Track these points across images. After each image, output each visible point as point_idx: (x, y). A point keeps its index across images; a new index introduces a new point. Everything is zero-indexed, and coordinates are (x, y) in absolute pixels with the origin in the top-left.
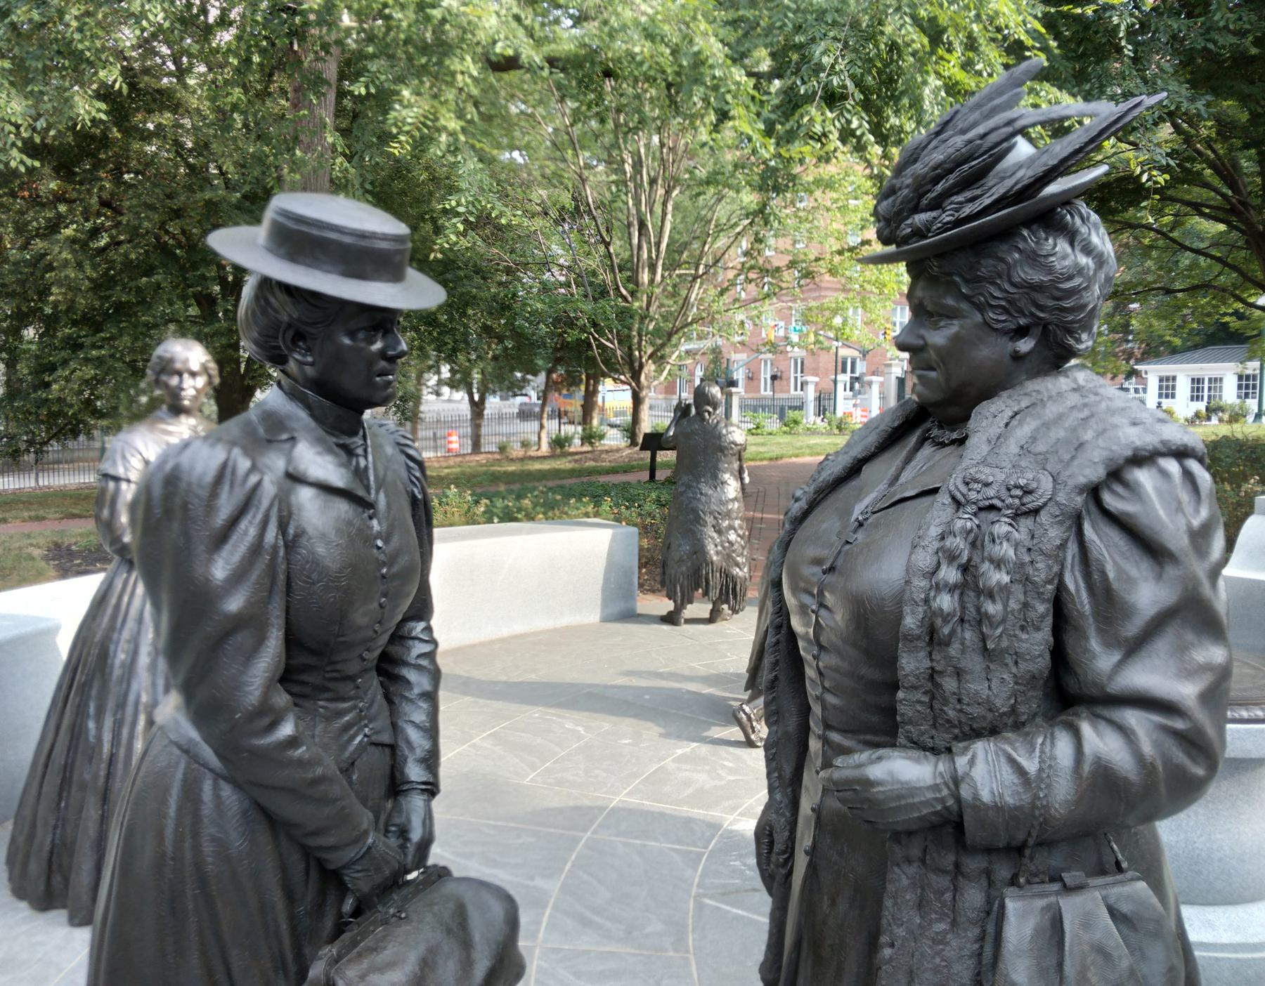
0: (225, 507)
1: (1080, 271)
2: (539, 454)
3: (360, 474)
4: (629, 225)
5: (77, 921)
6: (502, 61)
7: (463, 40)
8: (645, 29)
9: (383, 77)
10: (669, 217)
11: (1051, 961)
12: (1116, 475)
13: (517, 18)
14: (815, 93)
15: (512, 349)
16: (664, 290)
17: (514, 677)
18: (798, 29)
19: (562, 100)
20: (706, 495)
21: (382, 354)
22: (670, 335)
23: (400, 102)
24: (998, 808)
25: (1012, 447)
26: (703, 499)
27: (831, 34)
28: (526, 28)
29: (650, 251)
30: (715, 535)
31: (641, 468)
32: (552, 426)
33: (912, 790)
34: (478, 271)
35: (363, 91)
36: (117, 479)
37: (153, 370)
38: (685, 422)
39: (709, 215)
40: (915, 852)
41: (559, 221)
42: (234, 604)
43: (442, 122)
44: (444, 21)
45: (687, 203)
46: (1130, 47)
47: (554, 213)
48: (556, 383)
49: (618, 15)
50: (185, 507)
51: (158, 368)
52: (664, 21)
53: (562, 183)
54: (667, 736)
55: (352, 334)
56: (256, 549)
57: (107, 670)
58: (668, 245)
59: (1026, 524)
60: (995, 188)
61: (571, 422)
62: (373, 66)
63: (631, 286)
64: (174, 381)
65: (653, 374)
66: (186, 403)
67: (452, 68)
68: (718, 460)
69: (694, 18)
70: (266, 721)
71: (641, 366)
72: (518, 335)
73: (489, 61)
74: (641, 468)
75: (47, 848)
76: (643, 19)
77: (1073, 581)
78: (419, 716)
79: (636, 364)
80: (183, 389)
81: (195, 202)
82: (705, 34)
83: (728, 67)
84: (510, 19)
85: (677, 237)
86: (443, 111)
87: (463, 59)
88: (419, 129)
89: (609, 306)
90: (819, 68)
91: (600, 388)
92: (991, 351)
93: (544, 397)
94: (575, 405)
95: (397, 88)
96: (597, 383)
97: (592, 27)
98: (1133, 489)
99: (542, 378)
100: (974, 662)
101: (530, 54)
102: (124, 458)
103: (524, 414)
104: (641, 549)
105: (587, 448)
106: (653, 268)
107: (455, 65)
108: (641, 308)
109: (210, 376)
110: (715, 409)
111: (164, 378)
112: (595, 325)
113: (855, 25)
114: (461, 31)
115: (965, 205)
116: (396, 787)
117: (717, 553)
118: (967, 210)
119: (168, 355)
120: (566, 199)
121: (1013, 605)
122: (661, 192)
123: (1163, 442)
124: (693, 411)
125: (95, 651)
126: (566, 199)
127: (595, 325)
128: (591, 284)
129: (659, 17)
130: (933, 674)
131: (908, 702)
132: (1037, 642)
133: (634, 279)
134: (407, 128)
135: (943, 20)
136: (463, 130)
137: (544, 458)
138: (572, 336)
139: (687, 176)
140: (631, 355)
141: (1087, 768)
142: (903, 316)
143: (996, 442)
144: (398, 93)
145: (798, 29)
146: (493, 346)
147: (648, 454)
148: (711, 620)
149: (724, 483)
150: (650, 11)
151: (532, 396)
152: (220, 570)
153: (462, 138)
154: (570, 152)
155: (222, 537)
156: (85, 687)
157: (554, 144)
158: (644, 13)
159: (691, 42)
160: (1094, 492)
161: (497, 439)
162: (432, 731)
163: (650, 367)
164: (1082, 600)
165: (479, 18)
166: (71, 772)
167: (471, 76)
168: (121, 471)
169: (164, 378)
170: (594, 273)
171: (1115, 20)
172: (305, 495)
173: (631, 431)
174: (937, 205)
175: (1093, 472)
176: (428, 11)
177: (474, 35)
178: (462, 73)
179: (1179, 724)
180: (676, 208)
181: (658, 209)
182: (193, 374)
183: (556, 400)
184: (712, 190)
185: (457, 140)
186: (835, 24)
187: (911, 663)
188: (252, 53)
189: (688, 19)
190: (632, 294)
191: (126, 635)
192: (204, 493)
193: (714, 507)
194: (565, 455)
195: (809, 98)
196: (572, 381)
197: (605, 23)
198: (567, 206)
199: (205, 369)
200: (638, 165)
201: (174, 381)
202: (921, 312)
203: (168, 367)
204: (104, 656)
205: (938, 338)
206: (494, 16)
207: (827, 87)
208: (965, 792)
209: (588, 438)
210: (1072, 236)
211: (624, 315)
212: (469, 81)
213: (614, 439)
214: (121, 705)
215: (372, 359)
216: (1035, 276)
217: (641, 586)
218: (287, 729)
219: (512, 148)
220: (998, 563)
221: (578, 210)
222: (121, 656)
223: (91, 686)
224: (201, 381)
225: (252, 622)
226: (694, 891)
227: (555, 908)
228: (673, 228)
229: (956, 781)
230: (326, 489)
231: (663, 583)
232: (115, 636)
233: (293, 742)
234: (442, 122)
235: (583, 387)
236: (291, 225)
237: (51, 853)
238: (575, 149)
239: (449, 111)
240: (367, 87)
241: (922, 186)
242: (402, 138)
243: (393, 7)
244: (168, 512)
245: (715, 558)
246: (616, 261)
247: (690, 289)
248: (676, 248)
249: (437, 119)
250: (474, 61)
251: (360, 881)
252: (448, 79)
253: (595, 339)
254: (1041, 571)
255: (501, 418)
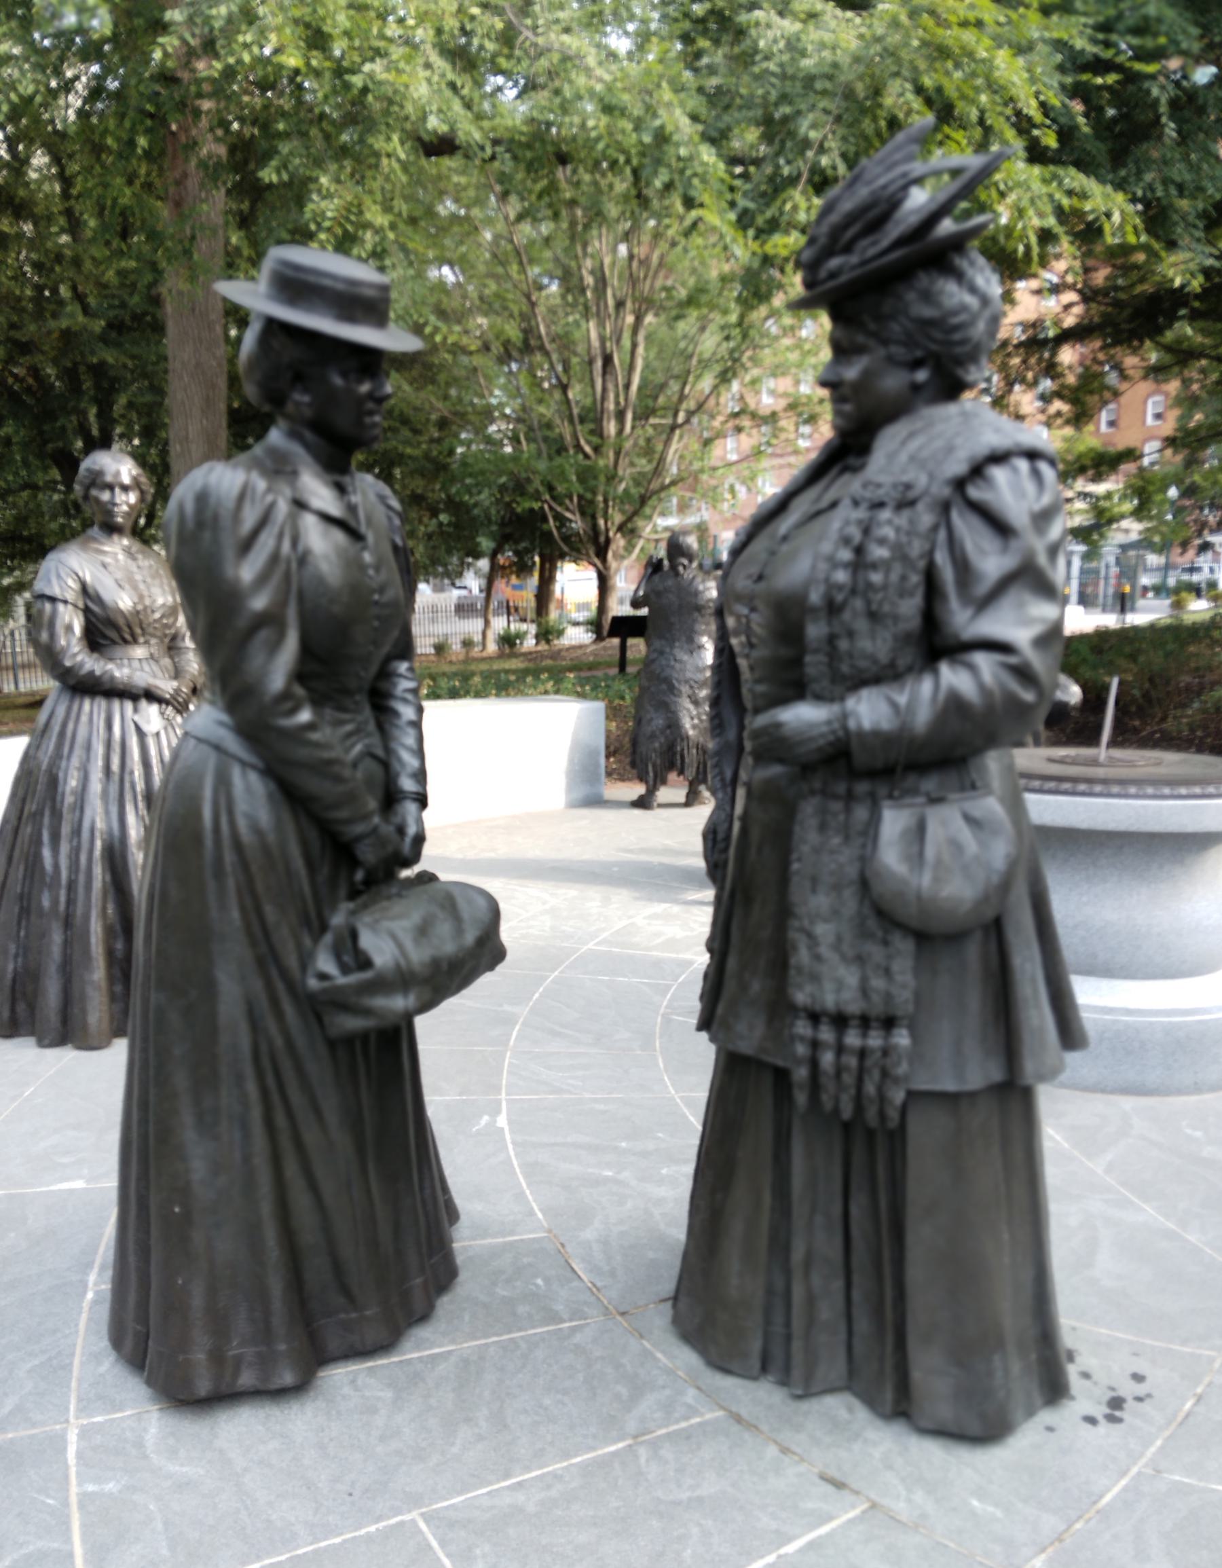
0: (250, 518)
1: (964, 308)
2: (485, 654)
3: (352, 509)
4: (591, 362)
5: (46, 1042)
6: (435, 141)
7: (386, 113)
8: (601, 100)
9: (297, 161)
10: (641, 350)
11: (915, 849)
12: (977, 471)
13: (452, 86)
14: (799, 175)
15: (449, 524)
16: (635, 445)
17: (471, 855)
18: (784, 98)
19: (504, 196)
20: (681, 662)
21: (370, 396)
22: (643, 500)
23: (319, 191)
24: (876, 734)
25: (903, 457)
26: (678, 666)
27: (821, 105)
28: (462, 98)
29: (617, 396)
30: (691, 707)
31: (609, 665)
32: (499, 624)
33: (812, 725)
34: (405, 421)
35: (275, 178)
36: (53, 600)
37: (81, 483)
38: (656, 578)
39: (690, 349)
40: (817, 784)
41: (506, 357)
42: (259, 603)
43: (368, 216)
44: (365, 90)
45: (663, 332)
46: (1172, 125)
47: (497, 348)
48: (503, 568)
49: (570, 82)
50: (216, 518)
51: (87, 481)
52: (624, 89)
53: (505, 308)
54: (637, 899)
55: (344, 375)
56: (275, 558)
57: (59, 798)
58: (640, 388)
59: (906, 514)
60: (894, 231)
61: (523, 620)
62: (285, 148)
63: (595, 440)
64: (105, 496)
65: (622, 551)
66: (120, 520)
67: (376, 146)
68: (695, 621)
69: (659, 86)
70: (288, 705)
71: (608, 541)
72: (454, 506)
73: (419, 139)
74: (609, 665)
75: (9, 976)
76: (599, 87)
77: (942, 558)
78: (410, 740)
79: (602, 539)
80: (115, 505)
81: (49, 333)
82: (669, 105)
83: (696, 145)
84: (444, 86)
85: (651, 377)
86: (368, 201)
87: (389, 139)
88: (341, 225)
89: (570, 464)
90: (806, 144)
91: (559, 576)
92: (893, 382)
93: (488, 590)
94: (526, 595)
95: (314, 174)
96: (553, 569)
97: (542, 97)
98: (989, 482)
99: (484, 564)
100: (862, 625)
101: (469, 132)
102: (59, 576)
103: (463, 609)
104: (608, 734)
105: (543, 647)
106: (620, 415)
107: (378, 143)
108: (607, 466)
109: (142, 492)
110: (691, 561)
111: (94, 492)
112: (551, 488)
113: (849, 94)
114: (385, 104)
115: (870, 248)
116: (391, 798)
117: (694, 727)
118: (872, 252)
119: (97, 467)
120: (513, 331)
121: (894, 577)
122: (630, 319)
123: (1018, 445)
124: (666, 563)
125: (43, 779)
126: (513, 331)
127: (551, 488)
128: (546, 439)
129: (619, 85)
130: (832, 639)
131: (814, 664)
132: (910, 607)
133: (599, 432)
134: (327, 224)
135: (951, 91)
136: (393, 226)
137: (490, 658)
138: (524, 505)
139: (663, 295)
140: (595, 526)
141: (942, 696)
142: (826, 354)
143: (891, 457)
144: (316, 180)
145: (784, 98)
146: (425, 520)
147: (616, 641)
148: (688, 804)
149: (701, 647)
150: (607, 77)
151: (473, 583)
152: (247, 572)
153: (391, 236)
154: (515, 267)
155: (247, 545)
156: (37, 816)
157: (495, 256)
158: (600, 80)
159: (655, 115)
160: (960, 484)
161: (432, 641)
162: (420, 753)
163: (619, 542)
164: (947, 574)
165: (407, 86)
166: (29, 900)
167: (399, 160)
168: (56, 591)
169: (94, 492)
170: (549, 426)
171: (1155, 92)
172: (310, 522)
173: (595, 625)
174: (848, 249)
175: (957, 467)
176: (347, 77)
177: (402, 107)
178: (389, 156)
179: (1012, 660)
180: (648, 338)
181: (626, 342)
182: (125, 489)
183: (503, 589)
184: (693, 314)
185: (384, 238)
186: (824, 93)
187: (815, 631)
188: (137, 133)
189: (650, 87)
190: (596, 449)
191: (75, 761)
192: (230, 504)
193: (689, 675)
194: (513, 655)
195: (793, 181)
196: (522, 569)
197: (557, 92)
198: (514, 339)
199: (136, 484)
200: (602, 282)
201: (105, 496)
202: (842, 350)
203: (97, 480)
204: (53, 782)
205: (851, 373)
206: (424, 84)
207: (815, 170)
208: (852, 724)
209: (546, 634)
210: (959, 276)
211: (586, 475)
212: (396, 165)
213: (577, 636)
214: (77, 832)
215: (361, 400)
216: (928, 312)
217: (609, 774)
218: (305, 716)
219: (442, 261)
220: (882, 541)
221: (529, 345)
222: (73, 783)
223: (42, 815)
224: (132, 498)
225: (271, 620)
226: (662, 1010)
227: (524, 1024)
228: (647, 366)
229: (845, 716)
230: (327, 518)
231: (633, 764)
232: (64, 764)
233: (311, 726)
234: (368, 216)
235: (536, 575)
236: (290, 273)
237: (14, 980)
238: (521, 263)
239: (375, 202)
240: (278, 172)
241: (837, 232)
242: (323, 236)
243: (306, 75)
244: (200, 524)
245: (691, 732)
246: (576, 411)
247: (667, 442)
248: (651, 391)
249: (361, 213)
250: (402, 143)
251: (368, 854)
252: (372, 161)
253: (551, 508)
254: (916, 548)
255: (434, 610)
